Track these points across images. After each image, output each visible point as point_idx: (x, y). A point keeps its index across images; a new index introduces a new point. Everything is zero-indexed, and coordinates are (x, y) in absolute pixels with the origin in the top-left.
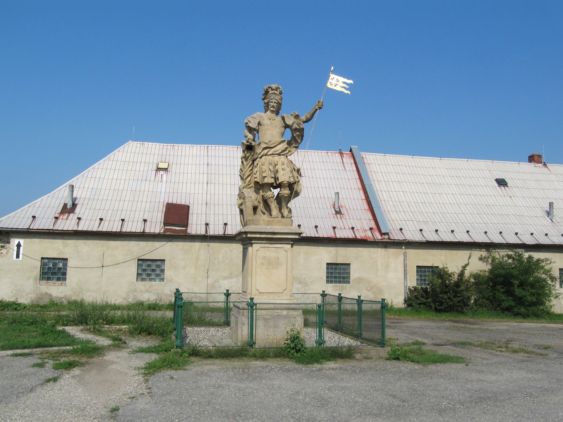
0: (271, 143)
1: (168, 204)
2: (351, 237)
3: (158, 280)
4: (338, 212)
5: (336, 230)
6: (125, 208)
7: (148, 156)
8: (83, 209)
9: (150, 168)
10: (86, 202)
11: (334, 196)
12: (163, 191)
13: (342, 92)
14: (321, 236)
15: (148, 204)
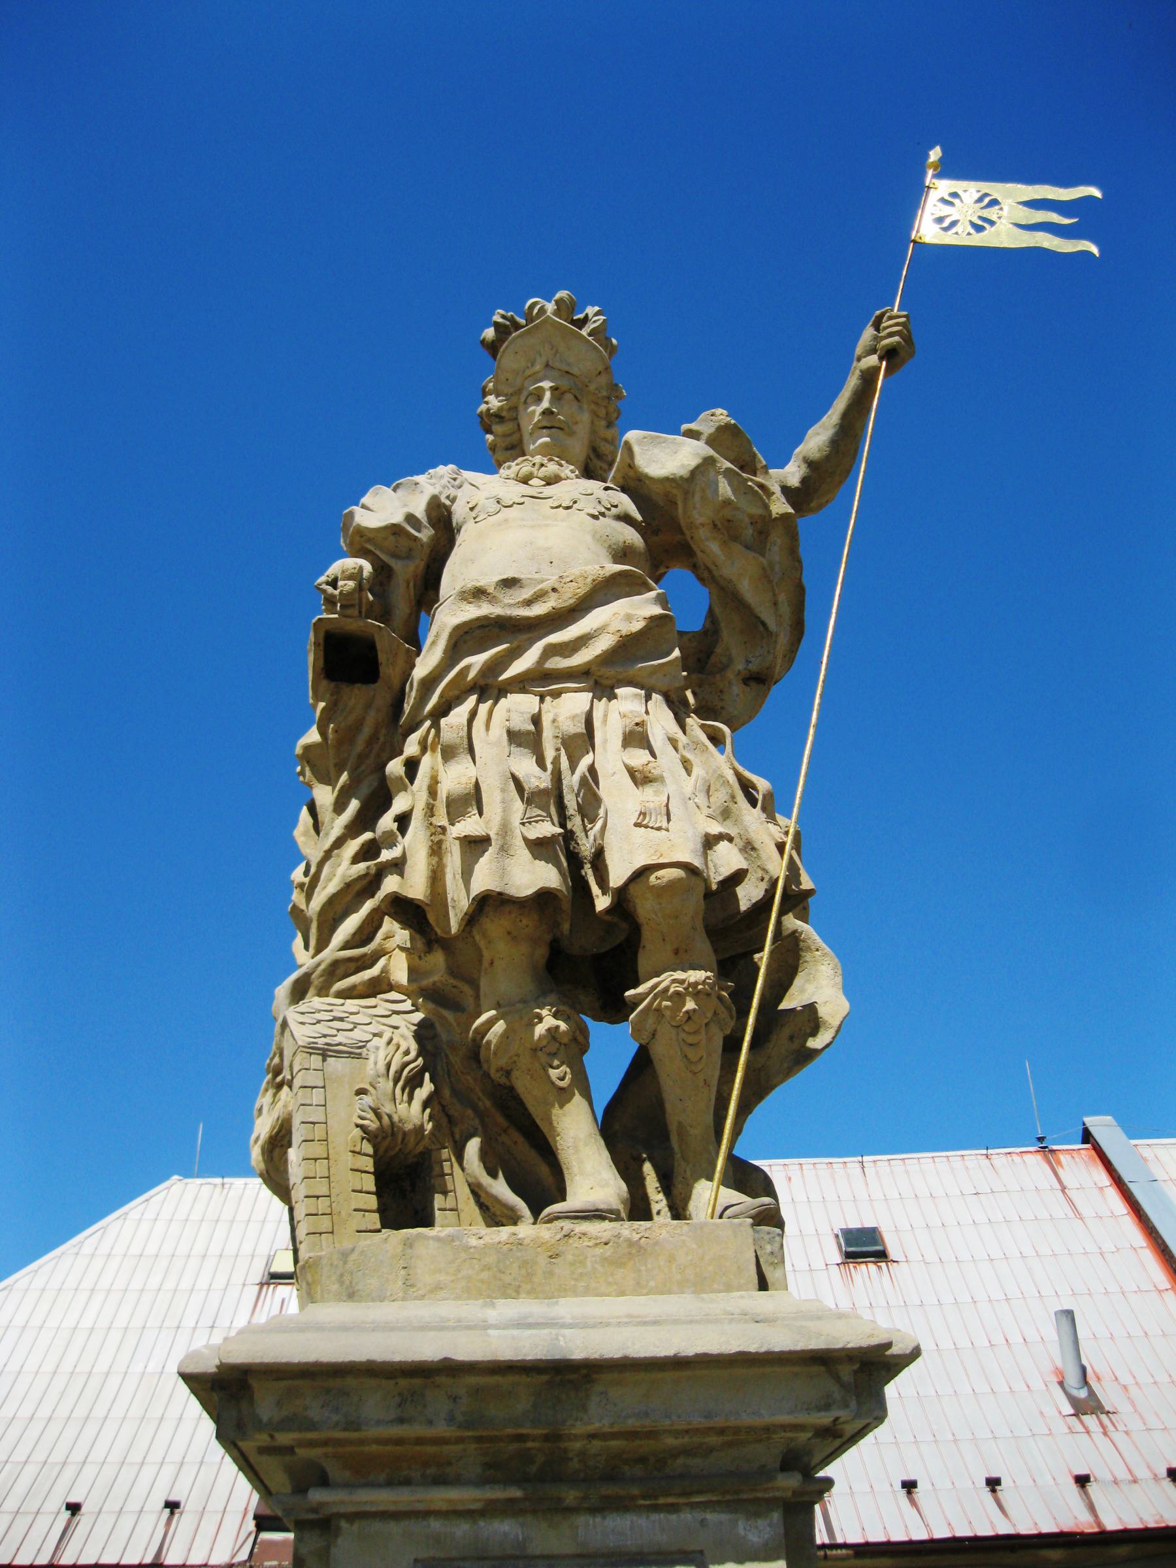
0: (526, 594)
4: (1087, 1406)
5: (1092, 1488)
9: (238, 1279)
14: (1025, 1528)
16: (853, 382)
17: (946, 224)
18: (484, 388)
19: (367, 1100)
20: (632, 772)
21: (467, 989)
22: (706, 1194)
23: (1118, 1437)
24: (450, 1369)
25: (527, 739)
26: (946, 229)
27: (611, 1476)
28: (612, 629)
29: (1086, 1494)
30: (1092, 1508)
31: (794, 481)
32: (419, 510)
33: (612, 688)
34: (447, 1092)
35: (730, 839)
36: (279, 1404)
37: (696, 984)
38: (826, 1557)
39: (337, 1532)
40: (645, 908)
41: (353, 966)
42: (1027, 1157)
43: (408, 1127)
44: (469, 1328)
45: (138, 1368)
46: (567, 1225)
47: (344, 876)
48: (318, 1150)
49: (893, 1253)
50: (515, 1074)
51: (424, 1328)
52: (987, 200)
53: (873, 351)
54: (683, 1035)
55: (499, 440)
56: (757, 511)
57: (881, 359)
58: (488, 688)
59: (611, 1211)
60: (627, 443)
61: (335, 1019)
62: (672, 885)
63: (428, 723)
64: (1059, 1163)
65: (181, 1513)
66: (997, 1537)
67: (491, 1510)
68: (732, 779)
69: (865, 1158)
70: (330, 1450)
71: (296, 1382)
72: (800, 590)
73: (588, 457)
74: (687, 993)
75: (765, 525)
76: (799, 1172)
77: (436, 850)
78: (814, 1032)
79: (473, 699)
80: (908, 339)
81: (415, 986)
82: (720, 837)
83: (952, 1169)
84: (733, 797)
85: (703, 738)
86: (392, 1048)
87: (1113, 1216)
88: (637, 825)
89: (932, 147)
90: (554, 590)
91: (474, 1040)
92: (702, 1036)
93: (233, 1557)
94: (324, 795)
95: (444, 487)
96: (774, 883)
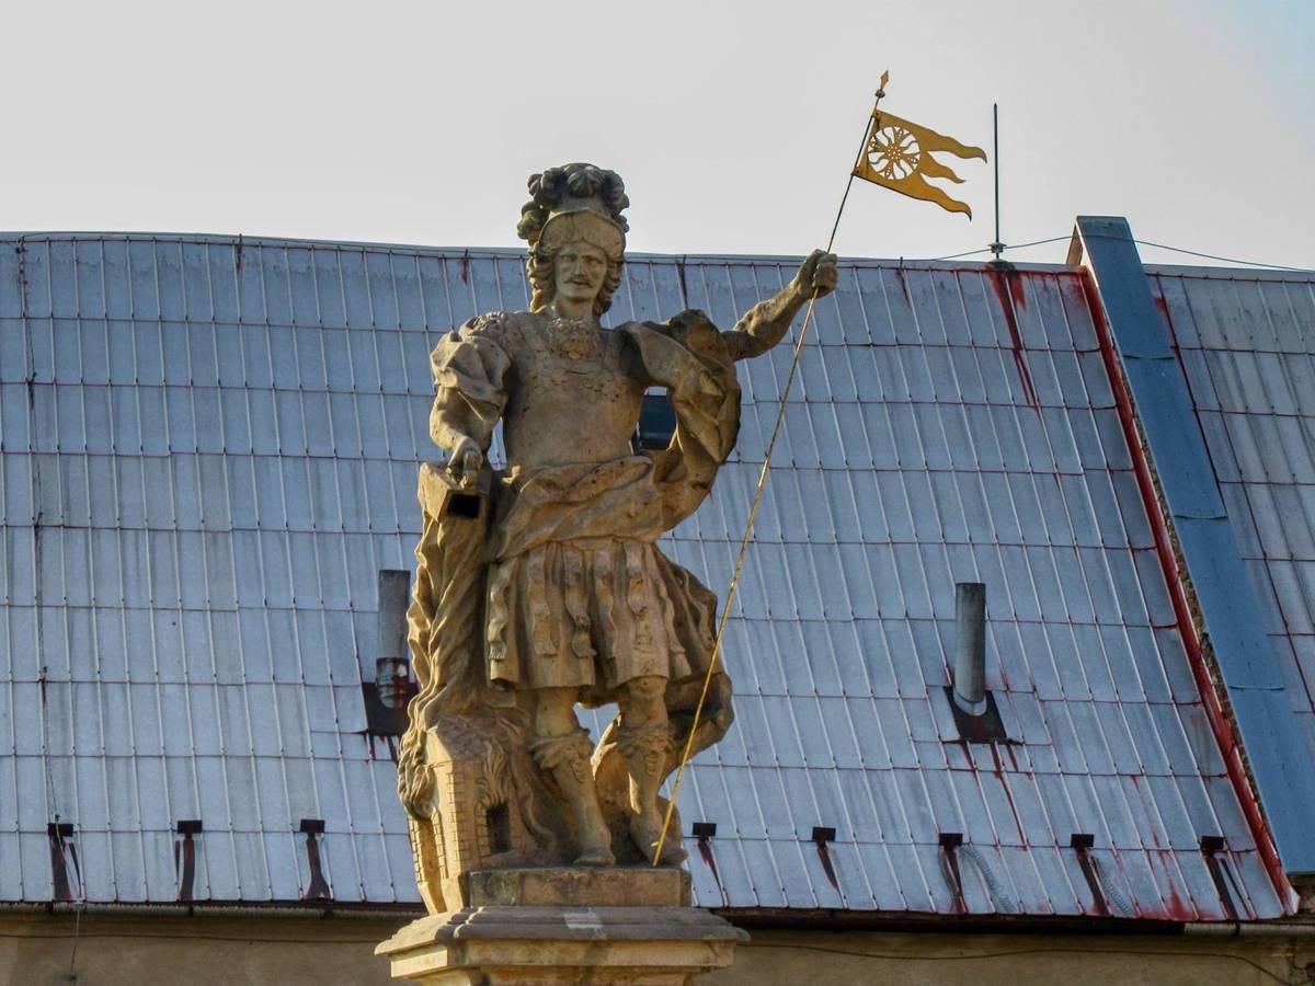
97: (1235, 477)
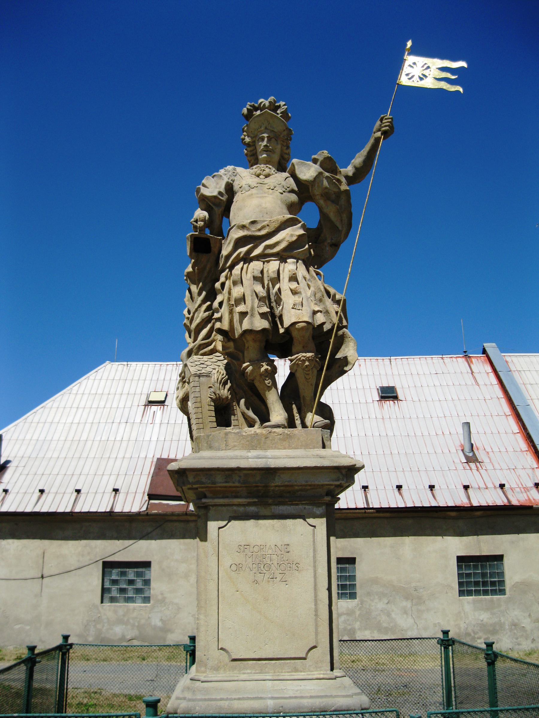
0: (259, 226)
1: (158, 459)
2: (499, 503)
3: (140, 600)
4: (472, 459)
5: (470, 490)
6: (85, 471)
7: (134, 383)
8: (17, 475)
10: (22, 464)
11: (460, 430)
12: (154, 438)
13: (441, 90)
14: (442, 504)
15: (126, 462)
16: (372, 141)
17: (410, 76)
18: (243, 129)
19: (212, 390)
20: (291, 290)
21: (241, 354)
22: (312, 418)
23: (483, 472)
24: (239, 469)
25: (259, 279)
26: (410, 79)
27: (281, 497)
28: (286, 239)
29: (467, 493)
30: (469, 498)
31: (350, 174)
32: (222, 190)
33: (287, 259)
34: (235, 386)
35: (321, 312)
36: (194, 478)
37: (309, 357)
38: (365, 512)
39: (210, 509)
40: (295, 334)
41: (205, 345)
42: (459, 359)
43: (224, 397)
44: (244, 458)
45: (98, 438)
46: (269, 429)
47: (202, 317)
48: (198, 405)
49: (400, 397)
50: (255, 381)
51: (232, 458)
52: (425, 66)
53: (379, 130)
54: (305, 371)
55: (249, 153)
56: (336, 190)
57: (382, 134)
58: (247, 259)
59: (282, 425)
60: (293, 164)
61: (202, 364)
62: (303, 328)
63: (227, 270)
64: (472, 362)
65: (119, 493)
66: (431, 507)
67: (249, 504)
68: (323, 289)
69: (392, 358)
70: (207, 489)
71: (198, 473)
72: (350, 214)
73: (280, 159)
74: (306, 360)
75: (340, 193)
76: (364, 363)
77: (231, 312)
78: (346, 365)
79: (242, 263)
80: (392, 127)
81: (224, 352)
82: (318, 311)
83: (427, 363)
84: (323, 296)
85: (315, 275)
86: (219, 373)
87: (491, 384)
88: (292, 308)
89: (407, 41)
90: (268, 225)
91: (243, 370)
92: (311, 372)
93: (140, 509)
94: (194, 289)
95: (230, 176)
96: (334, 325)
97: (530, 398)
